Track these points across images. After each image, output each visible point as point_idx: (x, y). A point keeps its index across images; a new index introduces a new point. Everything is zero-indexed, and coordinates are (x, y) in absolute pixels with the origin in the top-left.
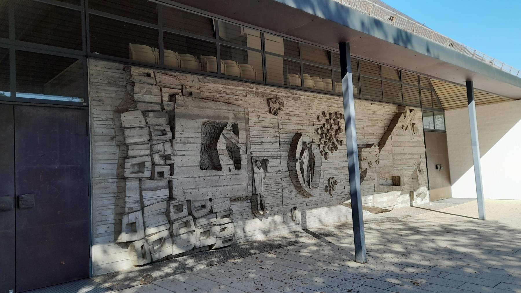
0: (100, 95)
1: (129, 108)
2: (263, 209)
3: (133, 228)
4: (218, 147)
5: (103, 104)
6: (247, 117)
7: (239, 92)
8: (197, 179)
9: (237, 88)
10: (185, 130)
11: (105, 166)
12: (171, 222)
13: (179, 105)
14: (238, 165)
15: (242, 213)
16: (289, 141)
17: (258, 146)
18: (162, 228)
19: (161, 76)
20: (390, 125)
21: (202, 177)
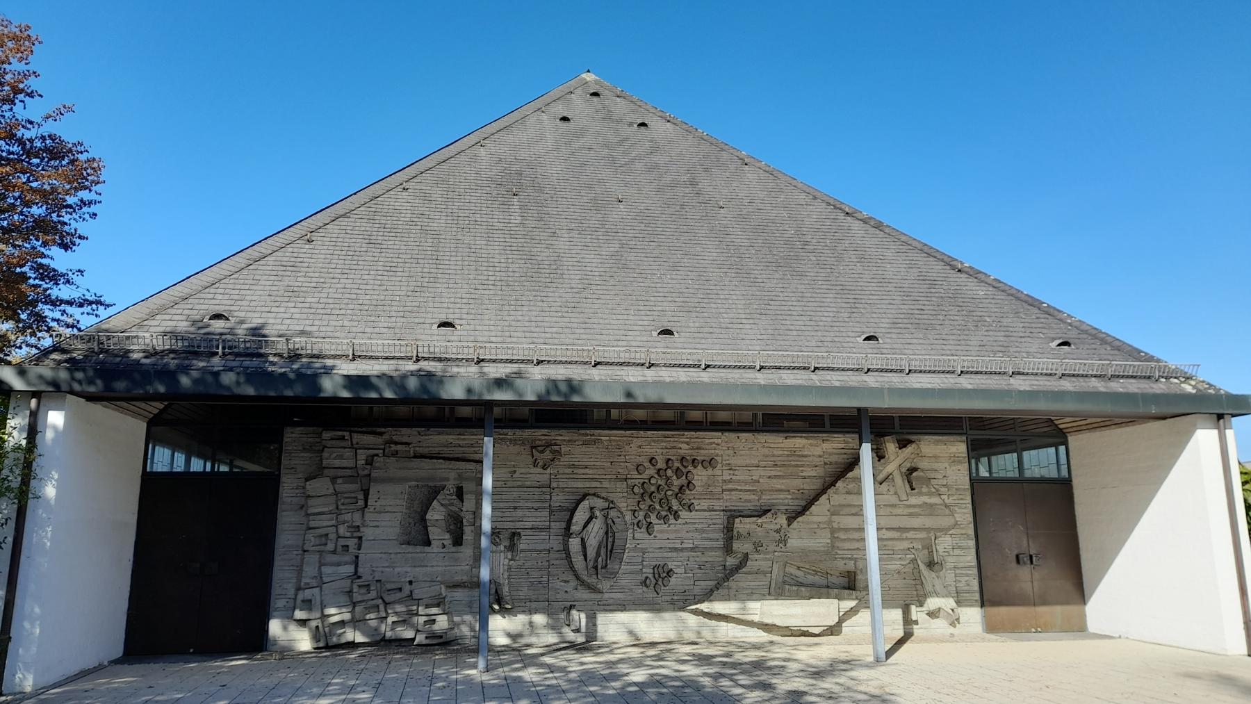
3: (308, 604)
4: (428, 517)
12: (354, 604)
18: (344, 610)
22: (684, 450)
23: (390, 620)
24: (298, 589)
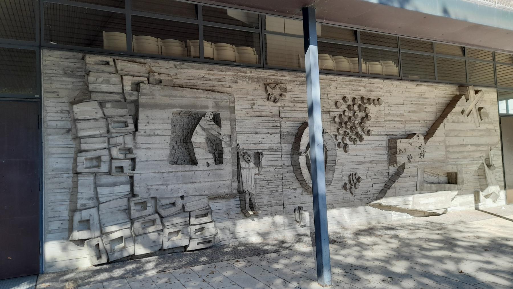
0: (54, 86)
1: (85, 99)
2: (252, 208)
3: (86, 224)
4: (193, 139)
5: (58, 95)
6: (232, 105)
7: (227, 77)
8: (165, 175)
9: (225, 73)
10: (151, 121)
11: (59, 160)
13: (144, 94)
14: (219, 159)
15: (228, 212)
16: (295, 131)
17: (250, 138)
19: (122, 64)
20: (445, 110)
21: (171, 172)
22: (363, 92)
23: (167, 231)
24: (74, 210)
